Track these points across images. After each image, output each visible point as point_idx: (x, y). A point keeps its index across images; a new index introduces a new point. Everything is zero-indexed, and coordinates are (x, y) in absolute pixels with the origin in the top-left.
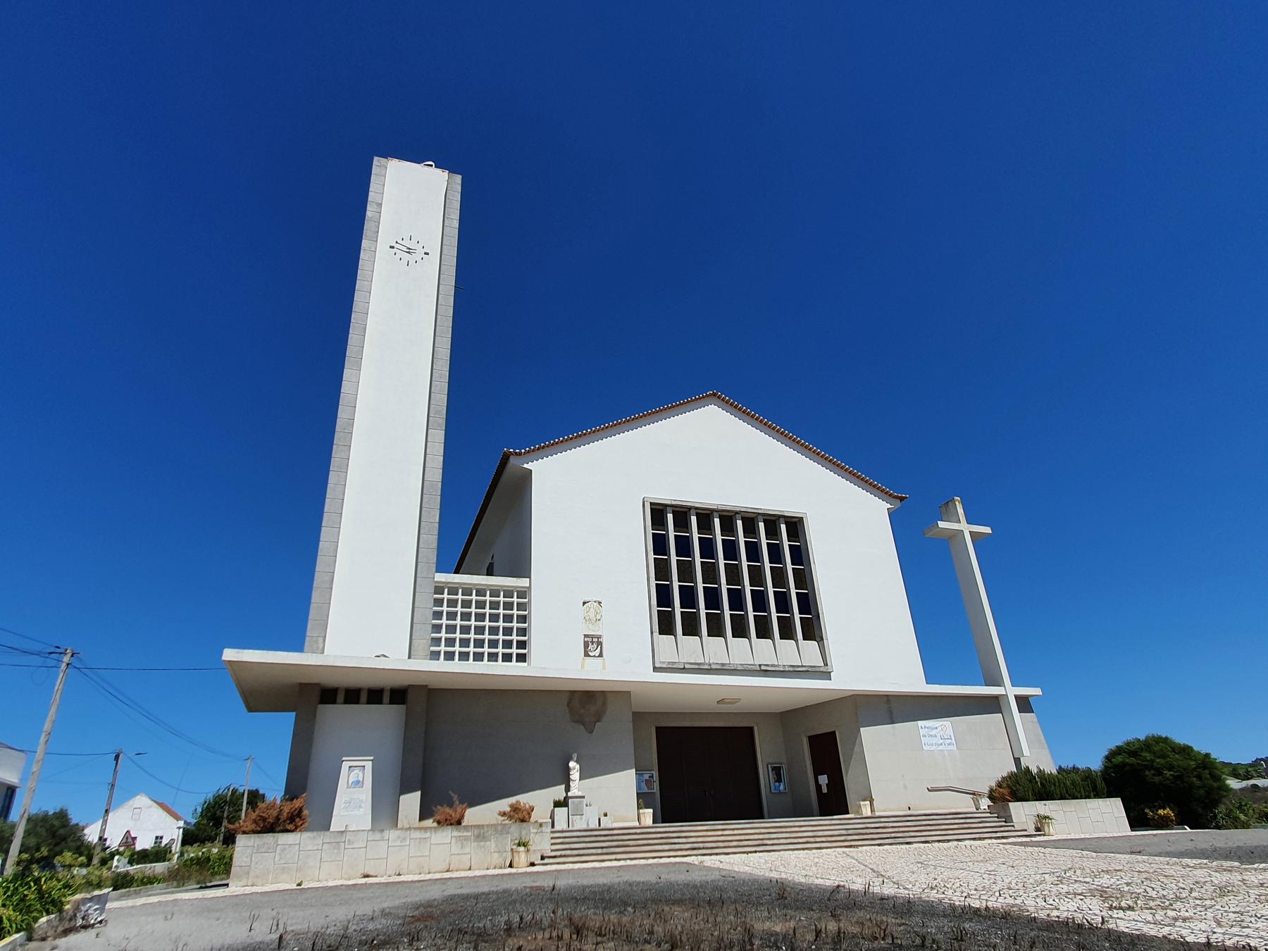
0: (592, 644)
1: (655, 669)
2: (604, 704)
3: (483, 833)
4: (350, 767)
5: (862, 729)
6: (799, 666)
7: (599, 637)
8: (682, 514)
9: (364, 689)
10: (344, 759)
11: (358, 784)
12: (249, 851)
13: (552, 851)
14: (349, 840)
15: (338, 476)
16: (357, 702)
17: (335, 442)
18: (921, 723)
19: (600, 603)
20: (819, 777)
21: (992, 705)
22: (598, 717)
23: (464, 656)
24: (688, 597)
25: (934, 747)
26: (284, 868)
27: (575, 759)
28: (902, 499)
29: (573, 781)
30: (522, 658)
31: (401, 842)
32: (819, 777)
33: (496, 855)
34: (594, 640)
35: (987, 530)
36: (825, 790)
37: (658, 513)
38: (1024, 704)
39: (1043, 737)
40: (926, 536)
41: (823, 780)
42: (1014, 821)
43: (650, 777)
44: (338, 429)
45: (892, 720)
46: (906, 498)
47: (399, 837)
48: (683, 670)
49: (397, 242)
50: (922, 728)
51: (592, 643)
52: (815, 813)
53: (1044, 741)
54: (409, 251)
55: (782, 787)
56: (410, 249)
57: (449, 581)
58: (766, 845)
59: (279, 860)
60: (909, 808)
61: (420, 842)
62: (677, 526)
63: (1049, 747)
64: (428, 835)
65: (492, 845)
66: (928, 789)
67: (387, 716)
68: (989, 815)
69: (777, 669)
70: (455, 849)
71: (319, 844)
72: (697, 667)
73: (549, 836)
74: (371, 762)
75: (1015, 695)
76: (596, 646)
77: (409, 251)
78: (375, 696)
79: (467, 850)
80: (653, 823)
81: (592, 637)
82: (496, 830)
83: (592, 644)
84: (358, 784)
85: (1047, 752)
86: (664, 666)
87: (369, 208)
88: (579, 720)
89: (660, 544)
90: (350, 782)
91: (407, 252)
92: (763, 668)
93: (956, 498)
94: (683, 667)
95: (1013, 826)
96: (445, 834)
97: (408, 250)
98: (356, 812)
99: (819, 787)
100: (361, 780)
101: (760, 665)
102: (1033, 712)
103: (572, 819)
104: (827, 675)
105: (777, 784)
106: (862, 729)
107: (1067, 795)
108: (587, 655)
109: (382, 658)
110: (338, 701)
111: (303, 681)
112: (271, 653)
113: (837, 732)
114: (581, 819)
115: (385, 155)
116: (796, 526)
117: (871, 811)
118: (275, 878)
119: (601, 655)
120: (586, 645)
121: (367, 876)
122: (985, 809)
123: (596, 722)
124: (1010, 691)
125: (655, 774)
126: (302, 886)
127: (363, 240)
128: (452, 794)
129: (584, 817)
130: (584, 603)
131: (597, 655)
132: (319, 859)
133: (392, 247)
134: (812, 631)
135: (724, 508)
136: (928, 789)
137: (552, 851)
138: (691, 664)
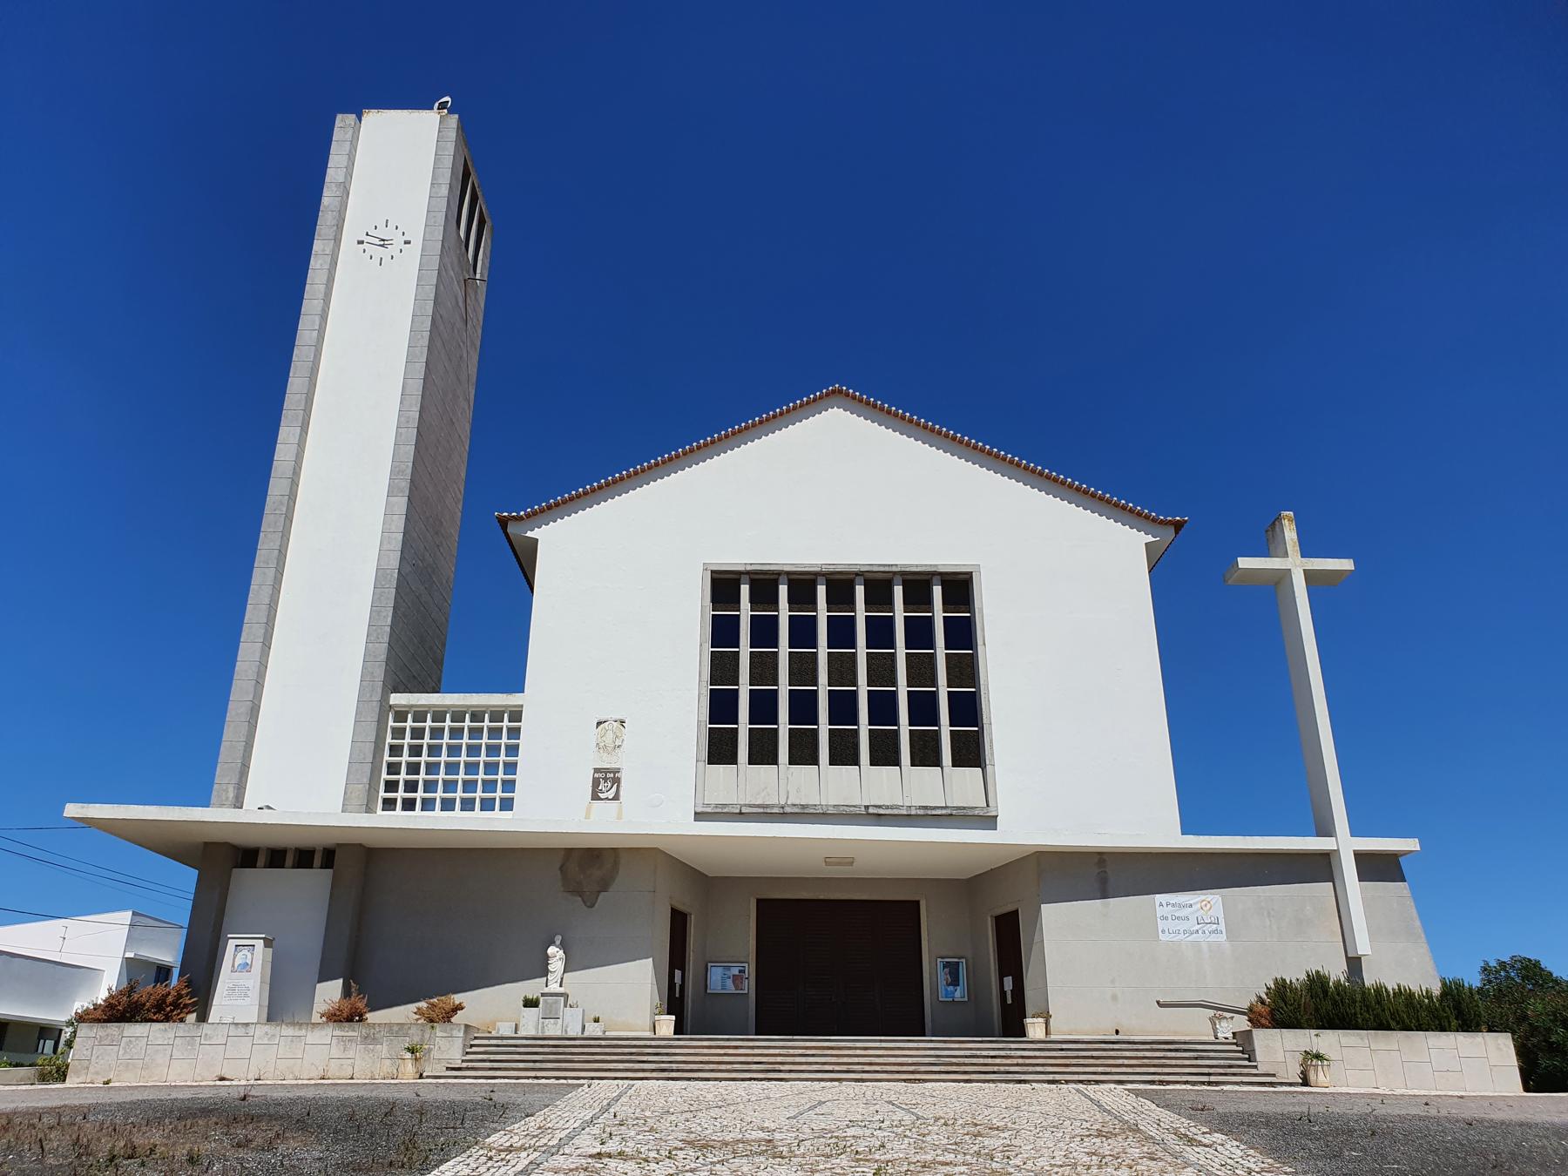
0: (606, 782)
1: (699, 816)
2: (616, 864)
3: (374, 1034)
4: (236, 946)
5: (1043, 906)
6: (942, 808)
7: (617, 771)
8: (764, 584)
9: (291, 849)
10: (229, 936)
11: (246, 967)
12: (90, 1042)
13: (463, 1061)
14: (206, 1035)
15: (265, 574)
16: (310, 866)
17: (262, 529)
18: (1159, 898)
19: (622, 722)
20: (1005, 979)
21: (1320, 867)
22: (604, 885)
23: (468, 805)
24: (764, 707)
25: (1181, 936)
26: (128, 1064)
27: (558, 942)
28: (1178, 526)
29: (551, 972)
30: (507, 805)
31: (269, 1039)
32: (1005, 979)
33: (388, 1062)
34: (609, 775)
35: (1346, 565)
36: (1009, 1001)
37: (723, 586)
38: (1376, 867)
39: (1418, 923)
40: (1230, 582)
41: (1008, 982)
42: (1258, 1060)
43: (740, 971)
44: (267, 510)
45: (1104, 895)
46: (1186, 521)
47: (267, 1033)
48: (741, 816)
49: (367, 234)
50: (1161, 905)
51: (606, 780)
52: (997, 1032)
53: (1420, 931)
54: (384, 243)
55: (958, 994)
56: (384, 240)
57: (413, 703)
58: (780, 1071)
59: (123, 1055)
60: (1117, 1032)
61: (292, 1041)
62: (908, 603)
63: (1429, 942)
64: (303, 1032)
65: (383, 1049)
66: (1158, 1002)
67: (317, 880)
68: (1234, 1047)
69: (896, 812)
70: (335, 1052)
71: (169, 1038)
72: (761, 810)
73: (458, 1044)
74: (262, 941)
75: (1354, 851)
76: (610, 785)
77: (384, 243)
78: (304, 857)
79: (351, 1054)
80: (675, 1034)
81: (606, 771)
82: (391, 1030)
83: (606, 782)
84: (246, 967)
85: (1423, 948)
86: (709, 810)
87: (326, 192)
88: (574, 889)
89: (724, 632)
90: (236, 966)
91: (380, 245)
92: (871, 810)
93: (1285, 513)
94: (738, 811)
95: (1256, 1067)
96: (324, 1033)
97: (382, 243)
98: (240, 1002)
99: (1003, 993)
100: (250, 963)
101: (867, 807)
102: (1404, 880)
103: (543, 1023)
104: (990, 822)
105: (951, 988)
106: (1043, 906)
107: (1393, 1024)
108: (595, 797)
109: (266, 811)
110: (258, 865)
111: (206, 841)
112: (123, 807)
113: (921, 903)
114: (556, 1024)
115: (358, 109)
116: (959, 588)
117: (1046, 1034)
118: (118, 1075)
119: (616, 797)
120: (596, 783)
121: (222, 1079)
122: (1226, 1038)
123: (599, 892)
124: (1346, 844)
125: (751, 969)
126: (111, 1085)
127: (315, 241)
128: (352, 984)
129: (560, 1021)
130: (599, 724)
131: (611, 797)
132: (169, 1056)
133: (361, 242)
134: (970, 752)
135: (832, 569)
136: (1158, 1002)
137: (463, 1061)
138: (750, 806)
